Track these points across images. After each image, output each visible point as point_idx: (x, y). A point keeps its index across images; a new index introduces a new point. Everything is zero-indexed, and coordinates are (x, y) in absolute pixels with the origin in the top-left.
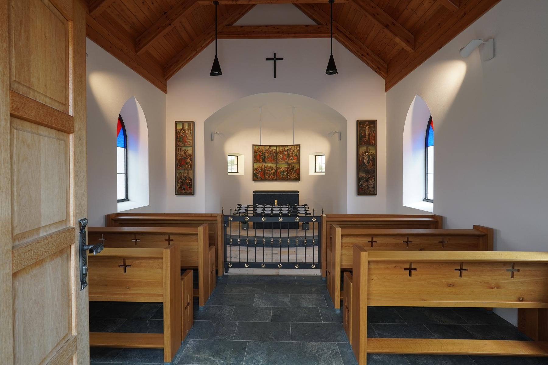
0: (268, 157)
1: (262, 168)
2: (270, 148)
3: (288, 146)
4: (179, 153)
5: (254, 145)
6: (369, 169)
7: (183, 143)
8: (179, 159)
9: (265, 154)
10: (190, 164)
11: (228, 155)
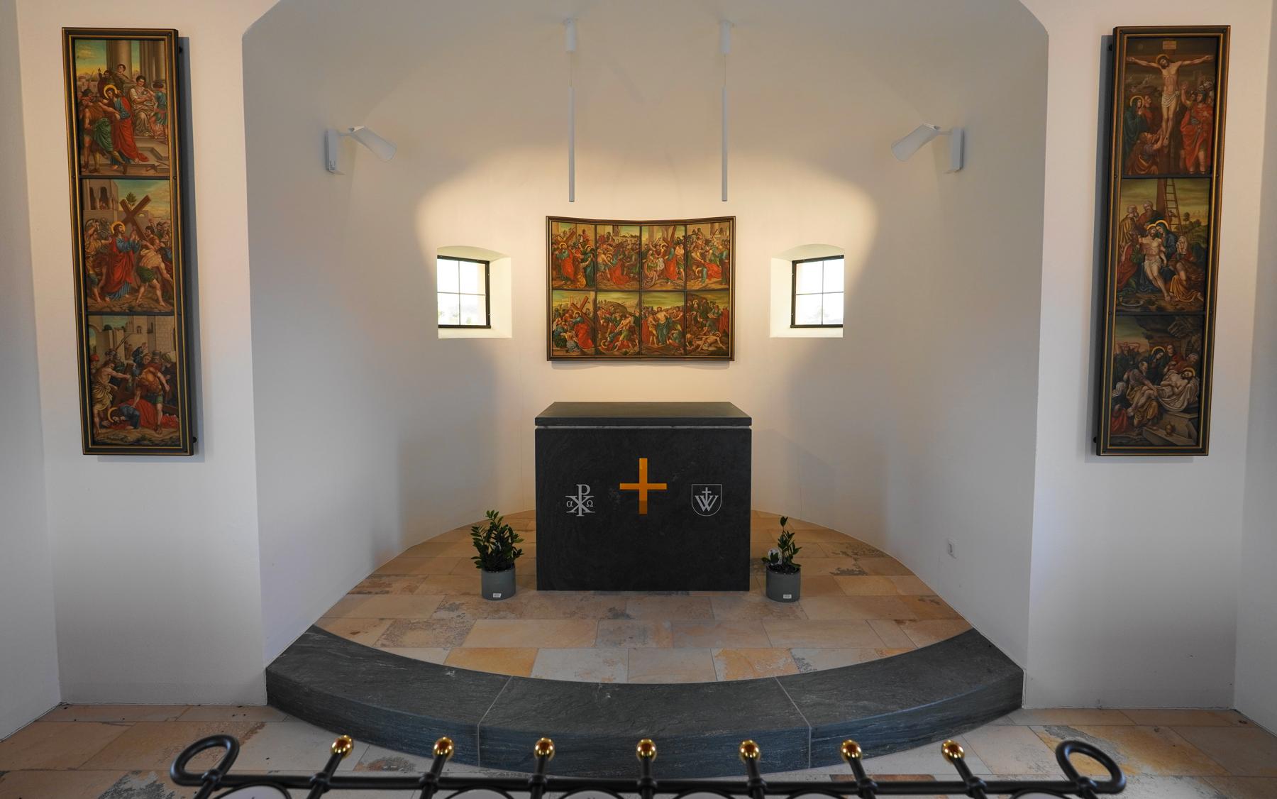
0: (606, 265)
1: (584, 311)
2: (617, 234)
3: (685, 223)
4: (99, 214)
5: (551, 219)
6: (1170, 308)
7: (114, 161)
8: (98, 252)
9: (596, 256)
10: (166, 286)
11: (439, 257)
